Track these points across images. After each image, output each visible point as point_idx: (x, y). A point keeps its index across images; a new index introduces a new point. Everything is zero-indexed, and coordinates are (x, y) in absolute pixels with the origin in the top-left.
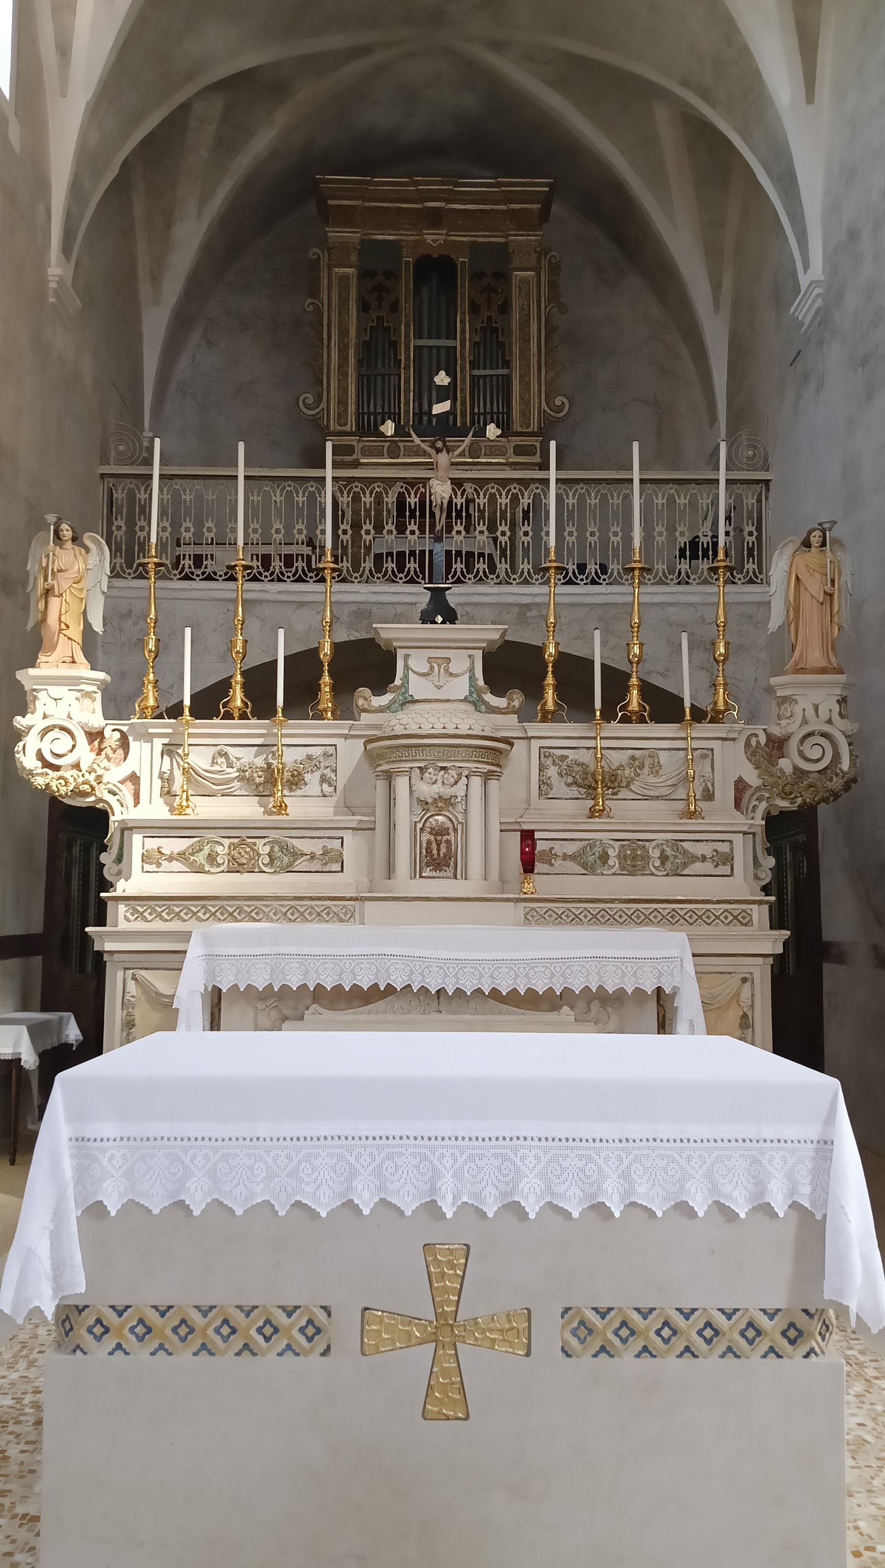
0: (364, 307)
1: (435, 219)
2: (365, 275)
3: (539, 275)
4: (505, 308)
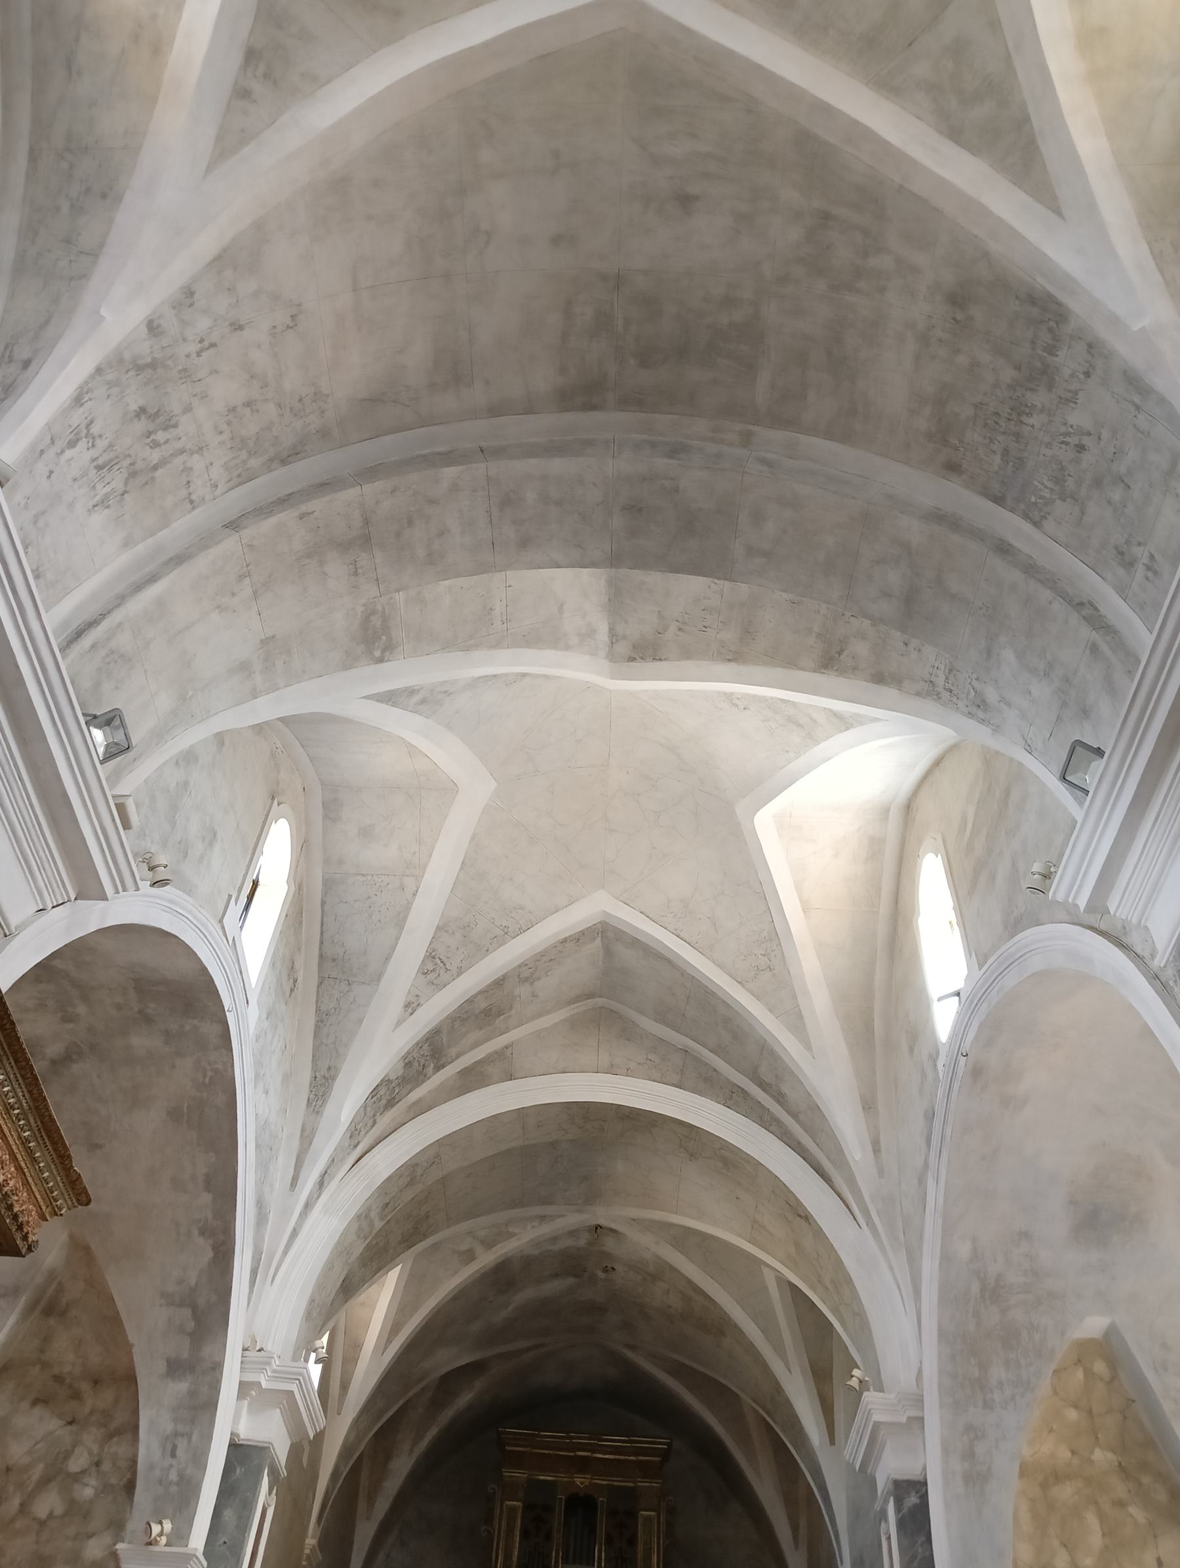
0: (525, 1534)
1: (583, 1465)
2: (528, 1507)
3: (659, 1517)
4: (632, 1541)
